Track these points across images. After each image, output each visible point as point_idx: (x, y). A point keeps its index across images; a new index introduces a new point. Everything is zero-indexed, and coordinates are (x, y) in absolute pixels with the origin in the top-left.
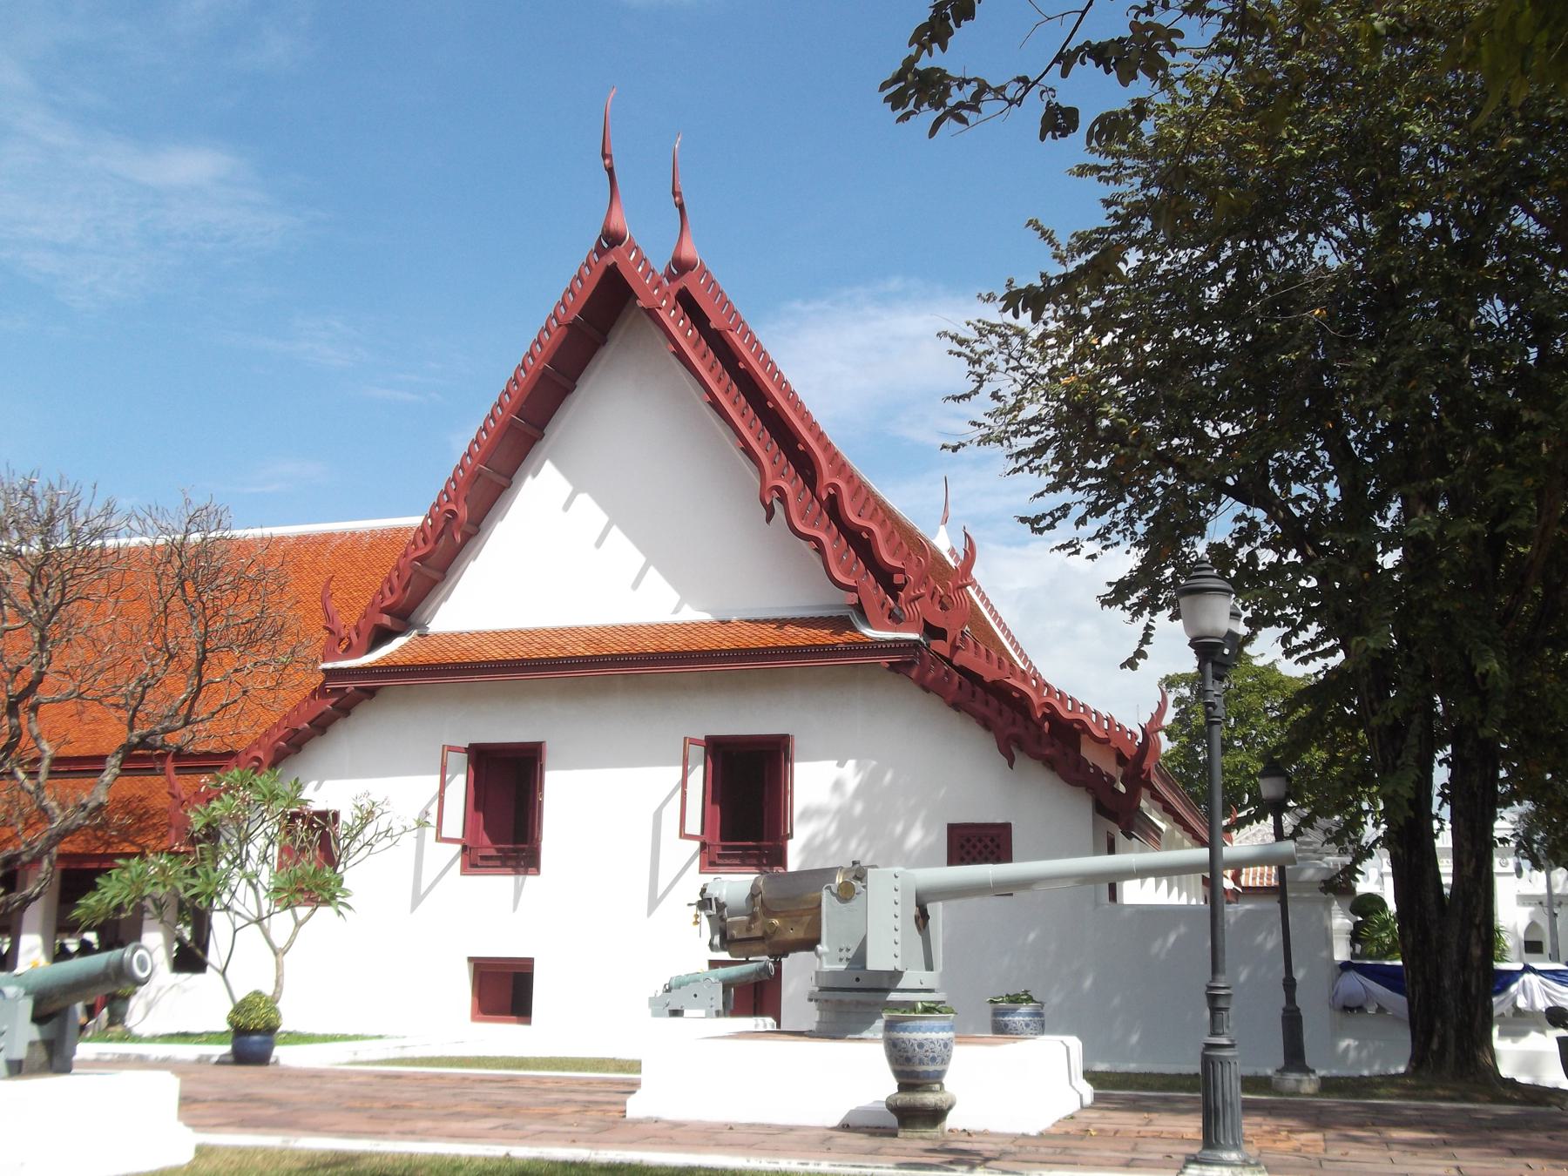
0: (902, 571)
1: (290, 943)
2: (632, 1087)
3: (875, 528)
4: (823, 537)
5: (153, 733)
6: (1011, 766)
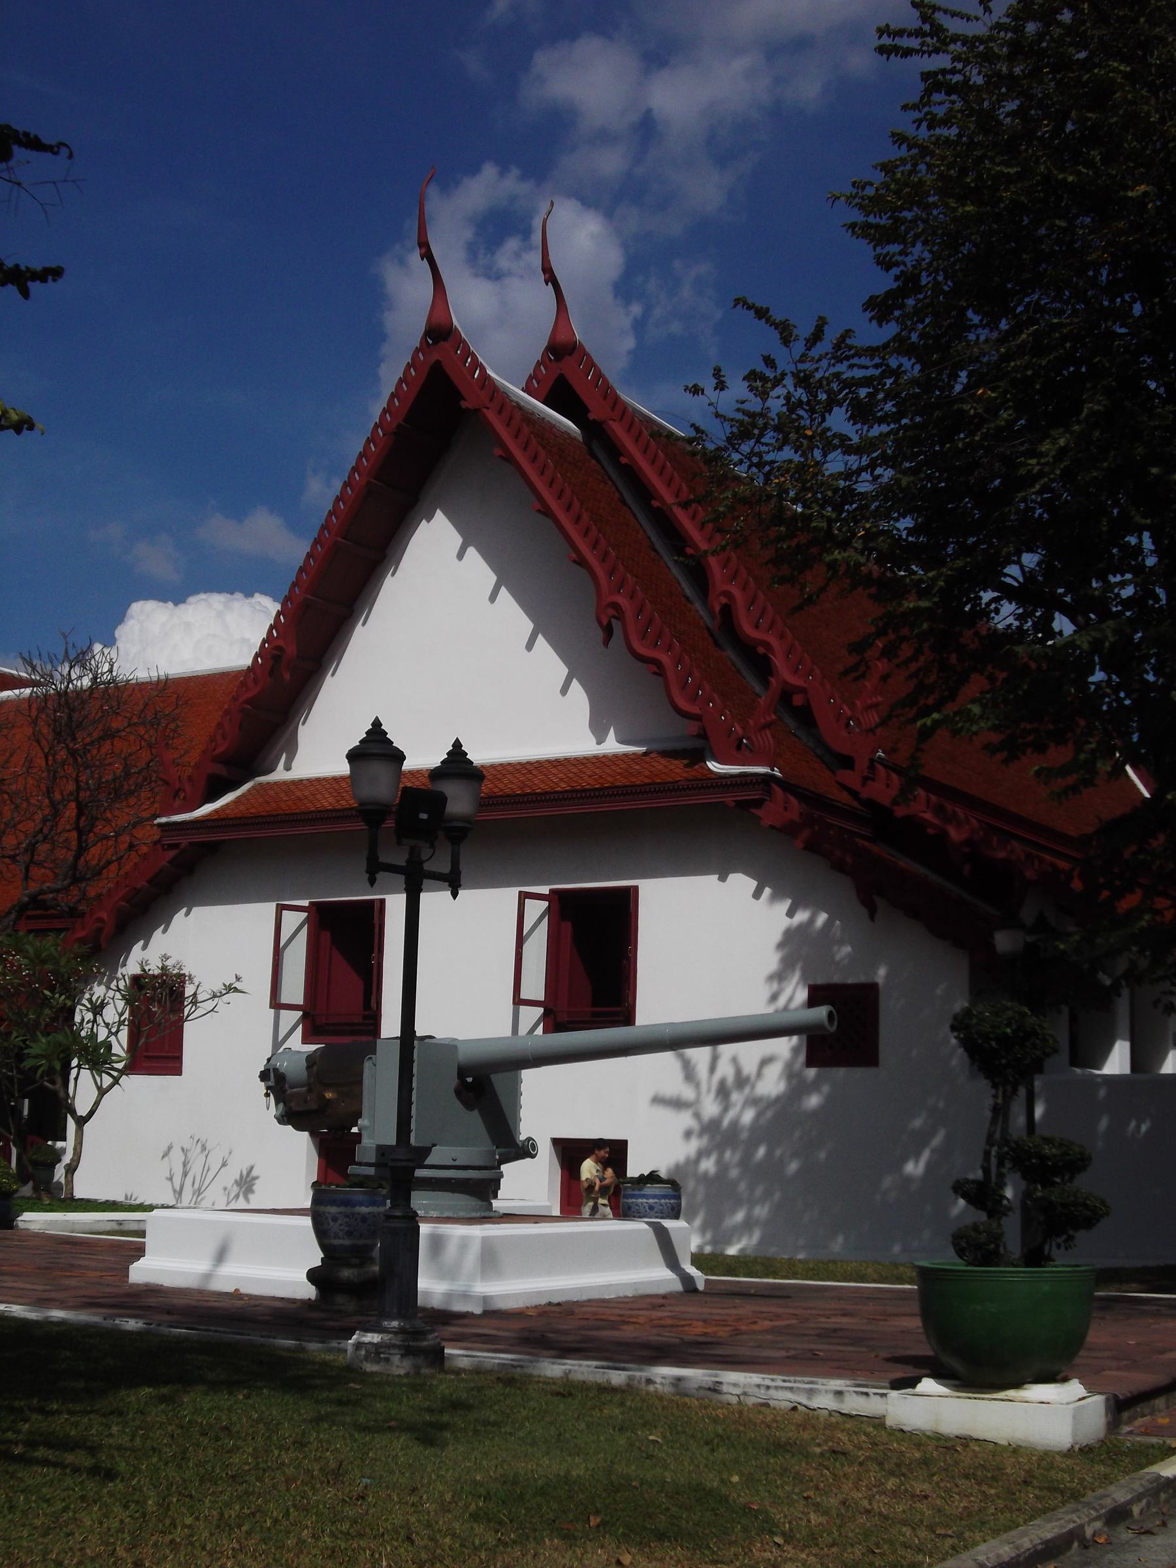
0: (803, 691)
1: (92, 1113)
2: (139, 1251)
3: (774, 642)
4: (665, 659)
5: (42, 892)
6: (872, 916)
